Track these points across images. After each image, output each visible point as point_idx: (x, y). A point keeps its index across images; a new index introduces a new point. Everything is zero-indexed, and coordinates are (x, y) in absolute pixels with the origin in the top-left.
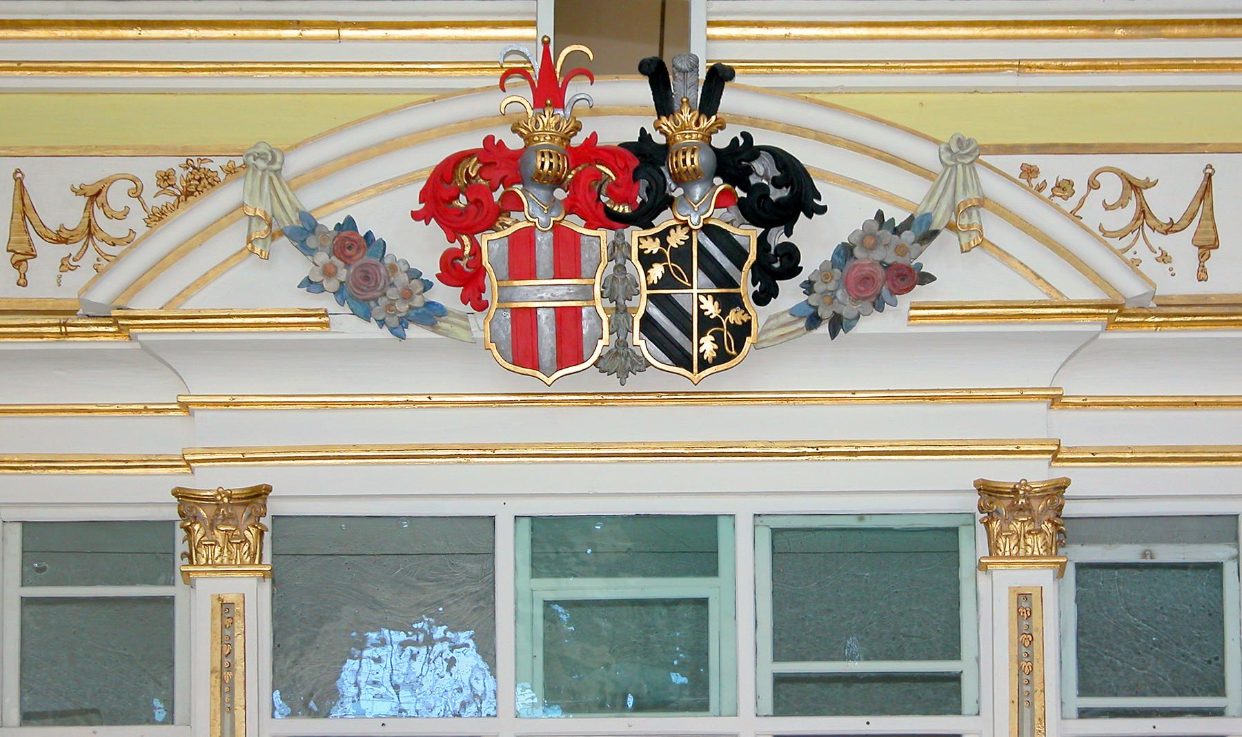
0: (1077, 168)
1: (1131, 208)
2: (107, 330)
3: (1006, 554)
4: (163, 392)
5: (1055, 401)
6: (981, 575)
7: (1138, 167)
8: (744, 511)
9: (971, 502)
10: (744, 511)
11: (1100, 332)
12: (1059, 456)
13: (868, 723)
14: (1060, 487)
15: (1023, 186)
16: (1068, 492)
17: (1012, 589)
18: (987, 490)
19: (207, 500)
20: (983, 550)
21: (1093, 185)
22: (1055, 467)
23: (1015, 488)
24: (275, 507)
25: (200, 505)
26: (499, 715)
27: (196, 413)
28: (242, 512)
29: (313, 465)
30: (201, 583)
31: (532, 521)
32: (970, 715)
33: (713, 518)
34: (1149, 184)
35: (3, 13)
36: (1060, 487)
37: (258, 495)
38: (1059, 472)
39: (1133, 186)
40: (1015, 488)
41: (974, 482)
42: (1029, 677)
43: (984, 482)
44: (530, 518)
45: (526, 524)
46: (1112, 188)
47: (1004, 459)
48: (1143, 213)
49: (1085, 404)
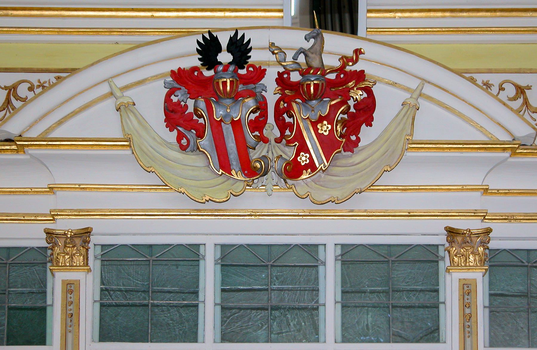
0: (495, 79)
1: (520, 101)
2: (463, 147)
3: (63, 265)
4: (43, 183)
5: (486, 191)
6: (447, 275)
7: (522, 80)
8: (330, 242)
9: (441, 239)
10: (330, 242)
11: (508, 158)
12: (486, 217)
13: (150, 347)
14: (488, 231)
15: (40, 94)
16: (491, 235)
17: (63, 281)
18: (452, 232)
19: (60, 235)
20: (448, 263)
21: (501, 89)
22: (486, 222)
23: (65, 233)
24: (94, 239)
25: (58, 237)
26: (336, 344)
27: (58, 193)
28: (78, 241)
29: (185, 219)
30: (454, 275)
31: (102, 247)
32: (201, 343)
33: (316, 246)
34: (529, 88)
35: (2, 3)
36: (488, 231)
37: (87, 232)
38: (487, 225)
39: (521, 91)
40: (65, 233)
41: (44, 229)
42: (469, 324)
43: (450, 228)
44: (101, 246)
45: (219, 248)
46: (511, 91)
47: (307, 219)
48: (526, 102)
49: (498, 192)
